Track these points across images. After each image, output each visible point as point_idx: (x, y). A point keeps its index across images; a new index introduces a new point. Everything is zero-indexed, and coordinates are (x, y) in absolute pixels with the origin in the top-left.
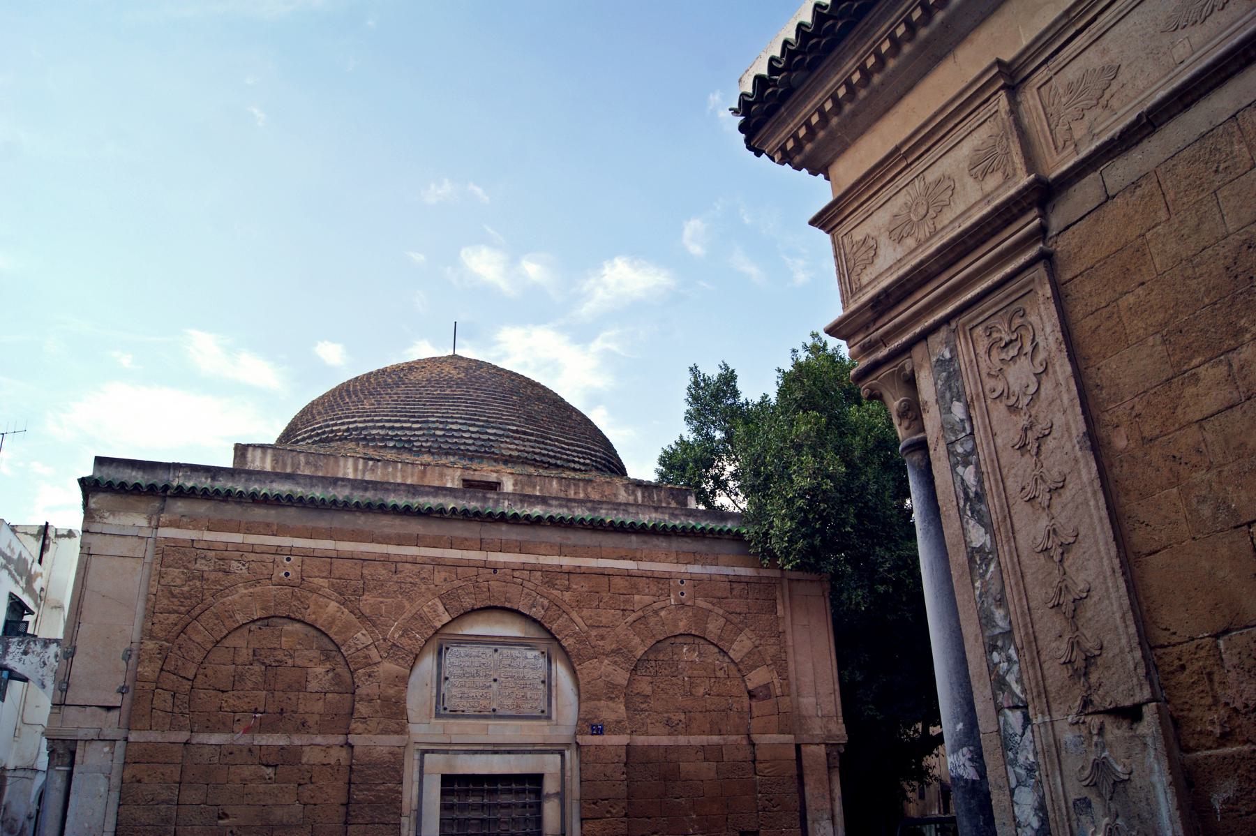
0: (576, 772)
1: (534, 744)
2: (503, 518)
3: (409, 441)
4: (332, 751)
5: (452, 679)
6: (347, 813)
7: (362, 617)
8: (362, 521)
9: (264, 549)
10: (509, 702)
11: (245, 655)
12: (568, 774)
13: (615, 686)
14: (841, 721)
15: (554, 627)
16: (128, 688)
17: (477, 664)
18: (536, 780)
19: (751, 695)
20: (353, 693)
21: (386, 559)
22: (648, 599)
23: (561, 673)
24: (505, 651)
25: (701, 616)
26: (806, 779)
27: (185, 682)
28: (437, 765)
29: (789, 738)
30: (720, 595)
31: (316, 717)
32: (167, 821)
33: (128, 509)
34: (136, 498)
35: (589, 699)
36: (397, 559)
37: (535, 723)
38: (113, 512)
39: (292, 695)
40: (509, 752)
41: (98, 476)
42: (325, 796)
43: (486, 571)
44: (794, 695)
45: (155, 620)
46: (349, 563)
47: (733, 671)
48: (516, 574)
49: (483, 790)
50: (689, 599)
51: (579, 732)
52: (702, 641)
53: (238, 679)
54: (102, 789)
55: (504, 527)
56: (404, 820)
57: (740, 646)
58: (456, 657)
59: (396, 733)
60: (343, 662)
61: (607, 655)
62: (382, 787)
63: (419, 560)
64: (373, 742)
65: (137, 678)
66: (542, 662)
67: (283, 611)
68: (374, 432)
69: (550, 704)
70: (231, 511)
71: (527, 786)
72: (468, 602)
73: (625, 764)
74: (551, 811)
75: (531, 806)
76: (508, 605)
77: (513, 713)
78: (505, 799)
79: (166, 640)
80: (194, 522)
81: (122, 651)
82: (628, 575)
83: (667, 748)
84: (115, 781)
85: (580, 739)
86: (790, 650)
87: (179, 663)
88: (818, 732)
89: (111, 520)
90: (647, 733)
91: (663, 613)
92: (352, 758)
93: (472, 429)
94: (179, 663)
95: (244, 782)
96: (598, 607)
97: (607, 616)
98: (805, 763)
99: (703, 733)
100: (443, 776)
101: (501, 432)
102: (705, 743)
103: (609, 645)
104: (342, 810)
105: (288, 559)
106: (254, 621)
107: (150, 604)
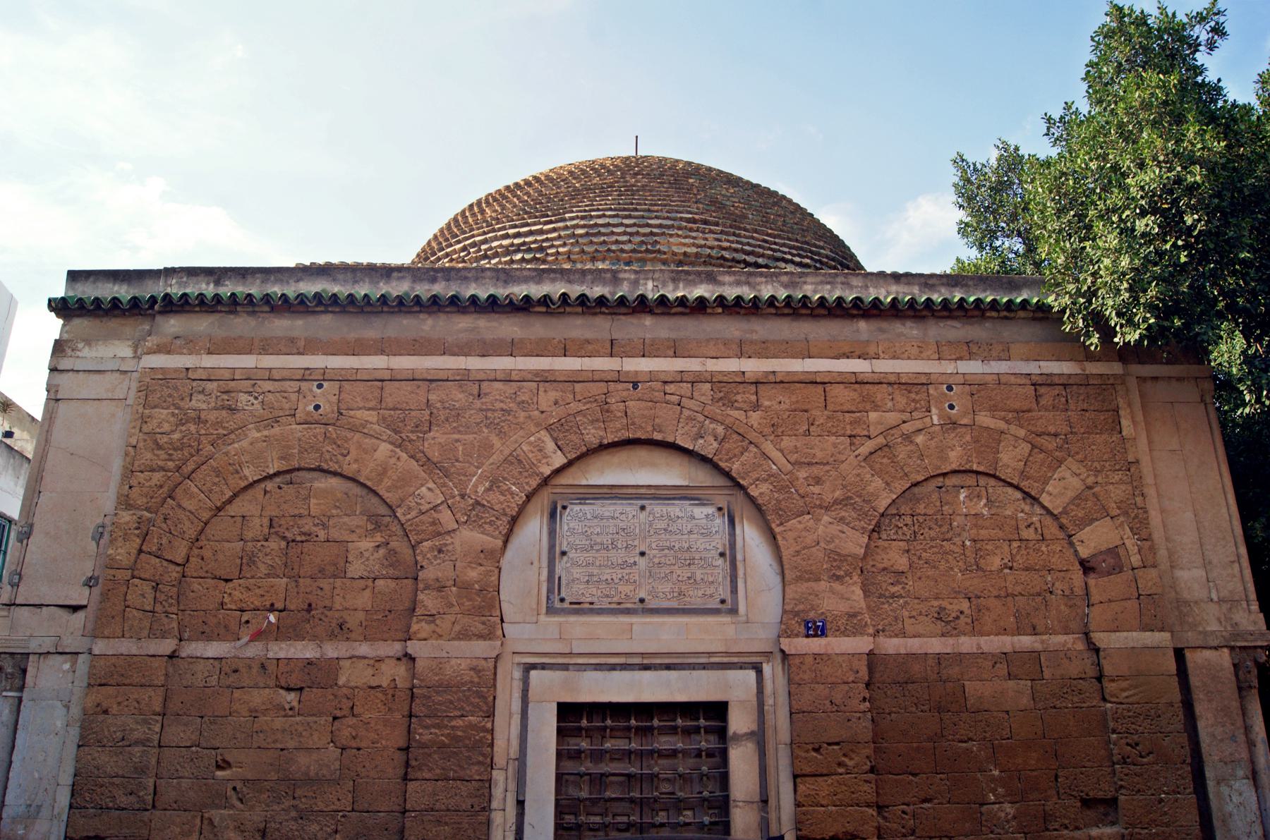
0: (783, 699)
1: (710, 654)
2: (642, 306)
3: (541, 249)
4: (383, 667)
5: (572, 554)
6: (407, 764)
7: (428, 463)
8: (428, 325)
9: (286, 374)
10: (667, 587)
11: (257, 526)
12: (769, 701)
13: (843, 558)
14: (1255, 607)
15: (735, 468)
16: (97, 579)
18: (718, 710)
19: (1087, 567)
20: (416, 579)
21: (463, 378)
22: (892, 418)
23: (750, 536)
25: (989, 441)
26: (1199, 709)
27: (172, 567)
28: (551, 689)
29: (1162, 638)
30: (1017, 405)
31: (361, 616)
32: (141, 770)
33: (108, 337)
34: (118, 320)
35: (799, 579)
36: (482, 376)
37: (710, 619)
38: (88, 342)
39: (325, 583)
40: (668, 667)
41: (71, 294)
42: (373, 736)
43: (620, 386)
44: (1164, 564)
45: (134, 482)
46: (408, 386)
47: (1052, 529)
48: (670, 388)
49: (629, 729)
50: (965, 414)
51: (786, 632)
52: (992, 482)
53: (247, 561)
54: (59, 724)
55: (648, 321)
56: (498, 775)
57: (1060, 488)
58: (575, 519)
59: (481, 637)
60: (400, 533)
61: (827, 509)
62: (459, 722)
63: (514, 377)
64: (446, 652)
65: (111, 565)
66: (720, 523)
67: (311, 460)
68: (495, 244)
69: (734, 590)
70: (242, 325)
71: (702, 722)
72: (593, 435)
73: (868, 685)
74: (741, 762)
75: (710, 754)
76: (658, 436)
77: (674, 604)
78: (665, 742)
79: (148, 510)
80: (189, 344)
81: (92, 527)
82: (857, 381)
83: (939, 658)
84: (76, 711)
85: (786, 644)
86: (1151, 492)
87: (164, 541)
88: (1214, 627)
89: (86, 352)
90: (903, 634)
91: (920, 439)
92: (414, 677)
93: (626, 221)
94: (164, 541)
95: (254, 714)
96: (808, 433)
97: (823, 447)
98: (1194, 681)
99: (1005, 631)
100: (560, 705)
101: (670, 223)
102: (1008, 649)
103: (830, 493)
104: (400, 757)
105: (320, 386)
106: (270, 477)
107: (128, 459)
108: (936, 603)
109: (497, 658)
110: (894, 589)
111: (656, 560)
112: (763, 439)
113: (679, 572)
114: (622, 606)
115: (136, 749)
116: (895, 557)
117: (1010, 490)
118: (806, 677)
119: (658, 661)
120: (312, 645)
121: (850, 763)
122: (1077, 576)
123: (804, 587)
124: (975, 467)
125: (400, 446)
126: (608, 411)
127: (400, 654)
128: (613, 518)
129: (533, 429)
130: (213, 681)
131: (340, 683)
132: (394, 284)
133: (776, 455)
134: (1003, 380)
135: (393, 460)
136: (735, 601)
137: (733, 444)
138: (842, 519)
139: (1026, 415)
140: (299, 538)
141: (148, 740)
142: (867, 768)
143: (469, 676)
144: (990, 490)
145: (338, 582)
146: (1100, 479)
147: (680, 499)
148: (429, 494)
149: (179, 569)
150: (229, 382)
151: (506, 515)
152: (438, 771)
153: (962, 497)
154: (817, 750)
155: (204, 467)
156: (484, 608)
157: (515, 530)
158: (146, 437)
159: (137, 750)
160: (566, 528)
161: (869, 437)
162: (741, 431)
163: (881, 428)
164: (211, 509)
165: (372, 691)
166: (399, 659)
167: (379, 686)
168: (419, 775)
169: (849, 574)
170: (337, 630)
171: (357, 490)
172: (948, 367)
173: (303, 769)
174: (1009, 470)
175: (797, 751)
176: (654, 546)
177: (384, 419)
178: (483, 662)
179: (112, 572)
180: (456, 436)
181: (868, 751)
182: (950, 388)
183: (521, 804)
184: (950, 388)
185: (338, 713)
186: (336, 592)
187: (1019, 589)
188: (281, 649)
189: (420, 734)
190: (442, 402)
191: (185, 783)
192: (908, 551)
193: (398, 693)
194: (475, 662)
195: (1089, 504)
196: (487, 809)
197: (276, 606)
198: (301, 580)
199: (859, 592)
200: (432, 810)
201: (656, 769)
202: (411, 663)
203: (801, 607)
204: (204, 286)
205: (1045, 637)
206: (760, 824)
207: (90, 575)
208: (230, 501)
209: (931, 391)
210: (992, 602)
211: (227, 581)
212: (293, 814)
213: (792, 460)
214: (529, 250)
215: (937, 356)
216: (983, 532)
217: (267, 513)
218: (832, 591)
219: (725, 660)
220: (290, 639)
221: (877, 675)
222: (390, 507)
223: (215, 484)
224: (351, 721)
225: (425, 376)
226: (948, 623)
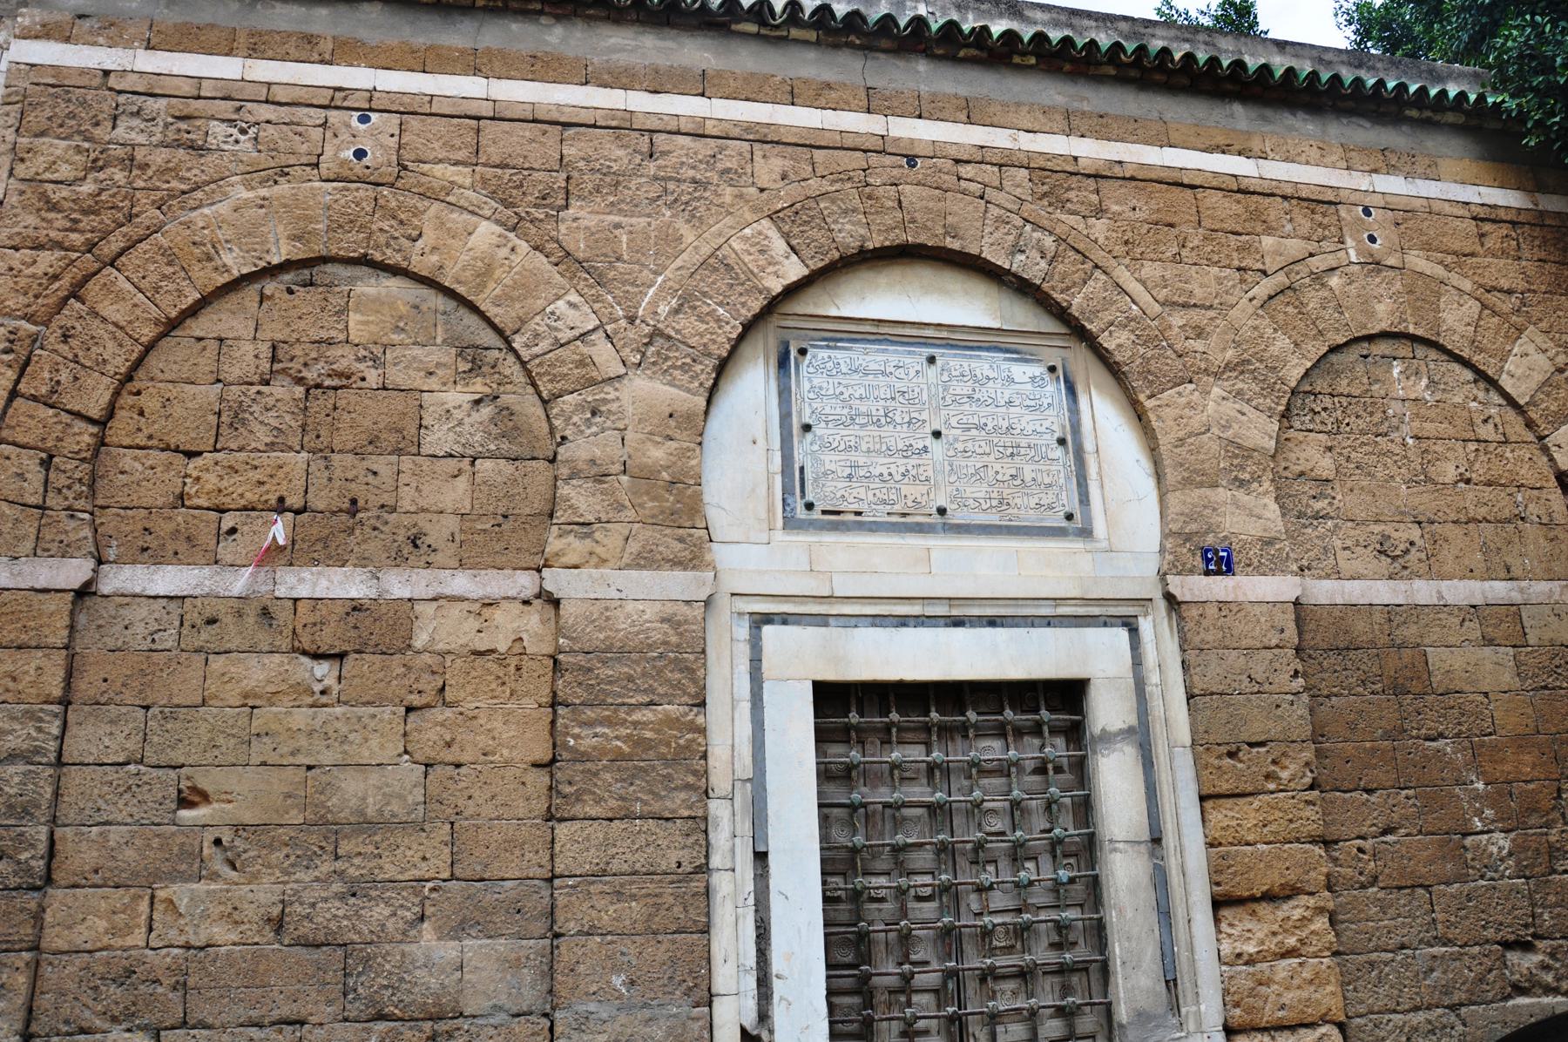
4: (498, 615)
5: (818, 430)
7: (566, 259)
10: (978, 491)
11: (247, 358)
12: (1154, 678)
13: (1247, 452)
15: (1077, 303)
17: (884, 392)
21: (622, 126)
22: (1295, 247)
23: (1104, 415)
25: (1423, 292)
27: (79, 425)
28: (802, 659)
30: (1456, 246)
31: (451, 523)
35: (1187, 482)
39: (382, 464)
40: (992, 622)
42: (483, 741)
43: (888, 160)
46: (528, 131)
47: (1516, 427)
48: (967, 171)
52: (1433, 354)
53: (230, 419)
56: (718, 809)
58: (825, 376)
59: (677, 563)
60: (520, 378)
62: (646, 715)
63: (710, 129)
64: (617, 590)
66: (1053, 391)
67: (350, 243)
69: (1084, 499)
72: (850, 233)
74: (1116, 780)
76: (955, 245)
77: (993, 519)
79: (29, 318)
82: (1240, 189)
83: (1390, 610)
85: (1176, 585)
87: (64, 376)
90: (1337, 574)
91: (1334, 281)
94: (64, 376)
97: (1203, 282)
102: (1478, 601)
106: (271, 271)
108: (1377, 528)
109: (708, 603)
111: (960, 447)
112: (1114, 262)
113: (997, 467)
114: (908, 520)
115: (11, 769)
116: (1312, 455)
117: (1456, 367)
118: (1210, 638)
119: (976, 612)
120: (360, 575)
121: (1285, 775)
124: (1411, 330)
125: (514, 229)
126: (870, 197)
127: (529, 593)
128: (883, 373)
129: (749, 216)
130: (168, 640)
131: (418, 643)
135: (504, 252)
136: (1088, 518)
138: (1239, 393)
139: (1470, 260)
140: (327, 382)
141: (37, 751)
142: (1308, 780)
143: (708, 557)
144: (1432, 366)
145: (407, 462)
147: (988, 349)
148: (571, 312)
149: (95, 429)
150: (189, 106)
151: (709, 355)
152: (613, 803)
153: (1396, 372)
154: (1231, 755)
155: (143, 246)
156: (675, 516)
157: (721, 383)
158: (23, 187)
160: (806, 385)
161: (1264, 273)
162: (1081, 247)
164: (157, 322)
165: (480, 661)
166: (526, 602)
167: (493, 651)
168: (577, 810)
171: (440, 302)
172: (1362, 181)
173: (353, 802)
174: (1456, 337)
176: (954, 422)
177: (485, 181)
178: (685, 609)
180: (617, 219)
181: (1308, 755)
182: (1367, 212)
183: (761, 857)
184: (1367, 212)
185: (415, 700)
186: (403, 478)
188: (301, 580)
189: (576, 737)
190: (587, 160)
191: (116, 834)
192: (1330, 449)
193: (527, 664)
194: (669, 609)
196: (704, 869)
197: (288, 502)
198: (335, 457)
200: (604, 873)
201: (977, 794)
202: (550, 610)
203: (1194, 527)
205: (1524, 584)
206: (1153, 877)
208: (193, 311)
209: (1343, 214)
210: (1451, 531)
211: (190, 455)
213: (1161, 297)
215: (1345, 165)
216: (1427, 425)
217: (268, 333)
219: (1081, 611)
220: (316, 562)
221: (1307, 636)
222: (499, 331)
223: (165, 277)
225: (555, 116)
226: (1394, 558)
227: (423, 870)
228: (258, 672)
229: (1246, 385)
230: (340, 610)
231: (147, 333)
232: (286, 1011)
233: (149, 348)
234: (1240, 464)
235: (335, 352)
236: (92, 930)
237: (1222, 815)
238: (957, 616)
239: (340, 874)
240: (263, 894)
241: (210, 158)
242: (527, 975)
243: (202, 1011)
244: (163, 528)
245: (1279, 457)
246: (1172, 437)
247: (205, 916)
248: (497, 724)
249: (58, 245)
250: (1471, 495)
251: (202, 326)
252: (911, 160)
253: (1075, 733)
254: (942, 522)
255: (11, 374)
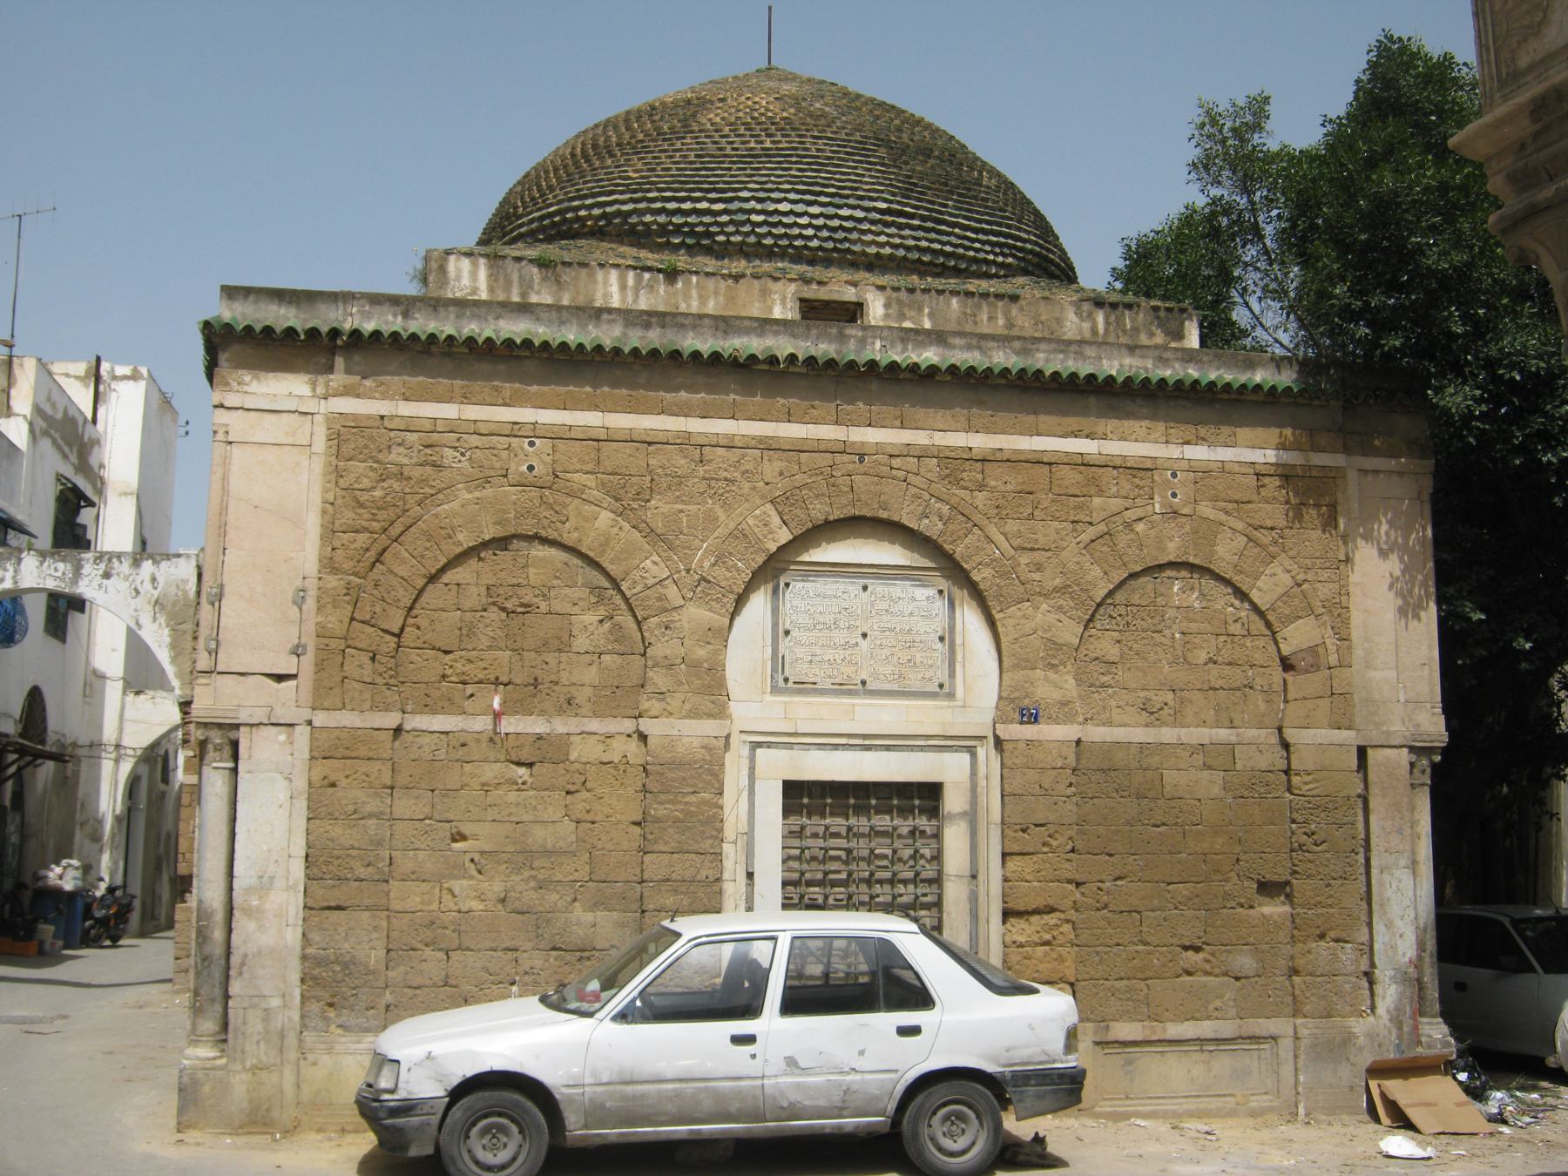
4: (615, 743)
9: (492, 428)
10: (888, 670)
11: (474, 596)
13: (1059, 646)
15: (959, 551)
16: (304, 647)
21: (684, 441)
22: (1115, 504)
23: (970, 620)
24: (880, 589)
25: (1207, 532)
27: (388, 637)
28: (779, 766)
31: (588, 691)
35: (1017, 666)
39: (551, 658)
40: (888, 748)
42: (607, 810)
43: (846, 458)
45: (337, 544)
48: (896, 462)
53: (467, 632)
56: (727, 848)
59: (711, 716)
62: (692, 799)
66: (940, 606)
69: (952, 674)
72: (820, 511)
74: (955, 840)
76: (883, 515)
77: (895, 687)
79: (355, 574)
82: (1082, 463)
83: (1142, 746)
84: (301, 784)
85: (1003, 731)
88: (1397, 727)
90: (1110, 723)
91: (1140, 527)
94: (378, 609)
95: (485, 787)
96: (1032, 517)
97: (1047, 531)
100: (785, 782)
107: (327, 518)
108: (1142, 694)
110: (1104, 679)
118: (1018, 762)
120: (541, 720)
121: (1055, 843)
122: (1277, 674)
123: (1020, 675)
124: (1191, 560)
127: (630, 731)
129: (758, 502)
130: (442, 754)
131: (572, 758)
132: (604, 327)
133: (999, 539)
134: (1227, 467)
135: (615, 530)
136: (953, 686)
137: (958, 524)
138: (1060, 607)
141: (382, 813)
142: (1069, 847)
145: (564, 657)
146: (1309, 577)
153: (1176, 589)
154: (1024, 831)
156: (710, 688)
159: (372, 822)
160: (788, 605)
163: (1103, 515)
168: (655, 848)
169: (1063, 663)
170: (565, 706)
172: (1174, 451)
175: (1009, 832)
177: (603, 484)
179: (325, 641)
180: (680, 507)
182: (1174, 475)
183: (750, 875)
184: (1174, 475)
185: (572, 788)
186: (563, 666)
187: (1221, 683)
193: (629, 769)
194: (706, 741)
195: (1297, 601)
196: (718, 880)
199: (1071, 681)
203: (1017, 694)
204: (390, 318)
207: (296, 641)
208: (443, 570)
210: (1196, 696)
212: (533, 884)
214: (692, 233)
218: (1046, 679)
221: (1083, 761)
224: (584, 795)
227: (576, 876)
228: (491, 772)
229: (1066, 602)
230: (531, 739)
231: (420, 582)
232: (508, 944)
233: (421, 591)
234: (1054, 655)
235: (521, 592)
236: (415, 902)
237: (1014, 864)
238: (867, 742)
239: (534, 877)
240: (498, 887)
241: (446, 473)
242: (628, 931)
243: (467, 943)
244: (436, 694)
245: (1082, 648)
246: (1010, 638)
247: (468, 897)
248: (614, 802)
249: (366, 530)
250: (1215, 672)
251: (448, 577)
252: (862, 456)
253: (934, 811)
254: (864, 689)
255: (350, 608)
